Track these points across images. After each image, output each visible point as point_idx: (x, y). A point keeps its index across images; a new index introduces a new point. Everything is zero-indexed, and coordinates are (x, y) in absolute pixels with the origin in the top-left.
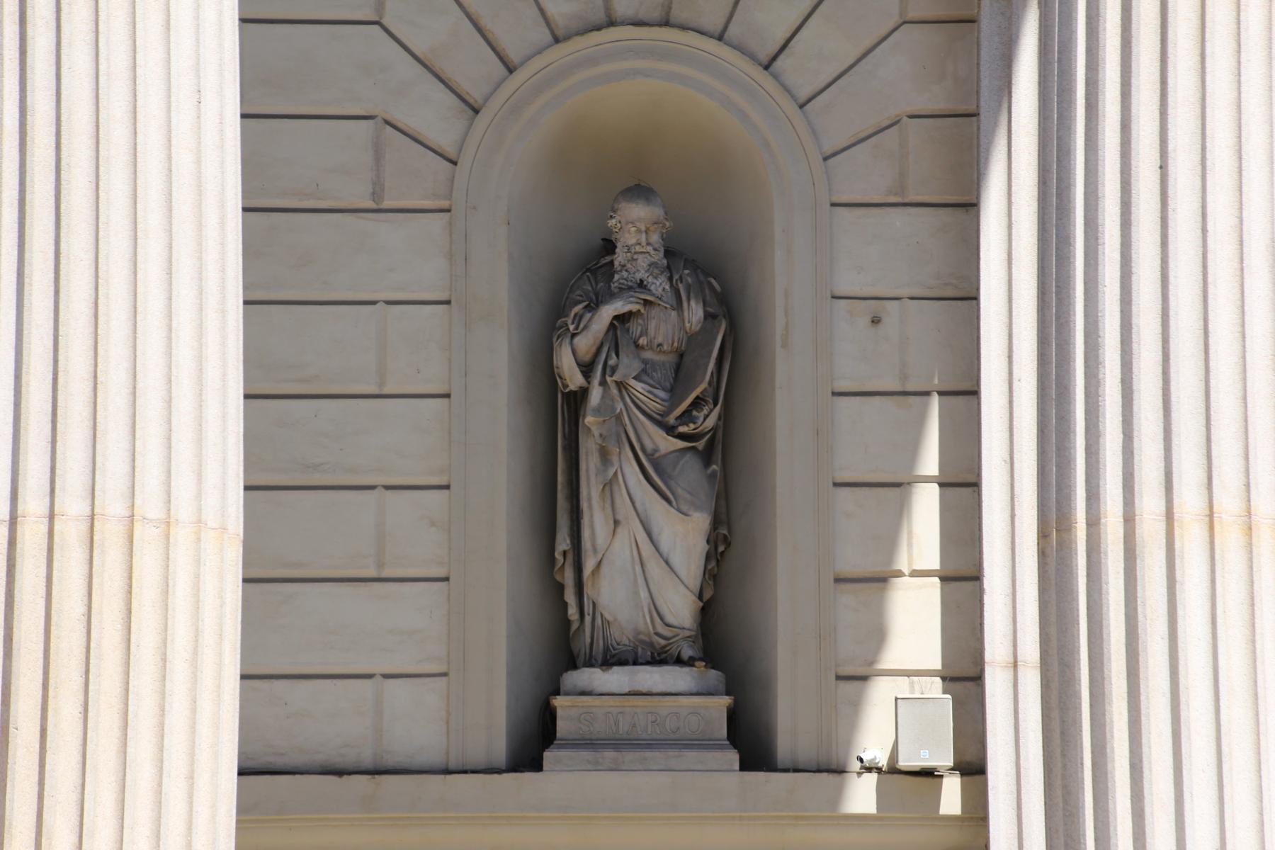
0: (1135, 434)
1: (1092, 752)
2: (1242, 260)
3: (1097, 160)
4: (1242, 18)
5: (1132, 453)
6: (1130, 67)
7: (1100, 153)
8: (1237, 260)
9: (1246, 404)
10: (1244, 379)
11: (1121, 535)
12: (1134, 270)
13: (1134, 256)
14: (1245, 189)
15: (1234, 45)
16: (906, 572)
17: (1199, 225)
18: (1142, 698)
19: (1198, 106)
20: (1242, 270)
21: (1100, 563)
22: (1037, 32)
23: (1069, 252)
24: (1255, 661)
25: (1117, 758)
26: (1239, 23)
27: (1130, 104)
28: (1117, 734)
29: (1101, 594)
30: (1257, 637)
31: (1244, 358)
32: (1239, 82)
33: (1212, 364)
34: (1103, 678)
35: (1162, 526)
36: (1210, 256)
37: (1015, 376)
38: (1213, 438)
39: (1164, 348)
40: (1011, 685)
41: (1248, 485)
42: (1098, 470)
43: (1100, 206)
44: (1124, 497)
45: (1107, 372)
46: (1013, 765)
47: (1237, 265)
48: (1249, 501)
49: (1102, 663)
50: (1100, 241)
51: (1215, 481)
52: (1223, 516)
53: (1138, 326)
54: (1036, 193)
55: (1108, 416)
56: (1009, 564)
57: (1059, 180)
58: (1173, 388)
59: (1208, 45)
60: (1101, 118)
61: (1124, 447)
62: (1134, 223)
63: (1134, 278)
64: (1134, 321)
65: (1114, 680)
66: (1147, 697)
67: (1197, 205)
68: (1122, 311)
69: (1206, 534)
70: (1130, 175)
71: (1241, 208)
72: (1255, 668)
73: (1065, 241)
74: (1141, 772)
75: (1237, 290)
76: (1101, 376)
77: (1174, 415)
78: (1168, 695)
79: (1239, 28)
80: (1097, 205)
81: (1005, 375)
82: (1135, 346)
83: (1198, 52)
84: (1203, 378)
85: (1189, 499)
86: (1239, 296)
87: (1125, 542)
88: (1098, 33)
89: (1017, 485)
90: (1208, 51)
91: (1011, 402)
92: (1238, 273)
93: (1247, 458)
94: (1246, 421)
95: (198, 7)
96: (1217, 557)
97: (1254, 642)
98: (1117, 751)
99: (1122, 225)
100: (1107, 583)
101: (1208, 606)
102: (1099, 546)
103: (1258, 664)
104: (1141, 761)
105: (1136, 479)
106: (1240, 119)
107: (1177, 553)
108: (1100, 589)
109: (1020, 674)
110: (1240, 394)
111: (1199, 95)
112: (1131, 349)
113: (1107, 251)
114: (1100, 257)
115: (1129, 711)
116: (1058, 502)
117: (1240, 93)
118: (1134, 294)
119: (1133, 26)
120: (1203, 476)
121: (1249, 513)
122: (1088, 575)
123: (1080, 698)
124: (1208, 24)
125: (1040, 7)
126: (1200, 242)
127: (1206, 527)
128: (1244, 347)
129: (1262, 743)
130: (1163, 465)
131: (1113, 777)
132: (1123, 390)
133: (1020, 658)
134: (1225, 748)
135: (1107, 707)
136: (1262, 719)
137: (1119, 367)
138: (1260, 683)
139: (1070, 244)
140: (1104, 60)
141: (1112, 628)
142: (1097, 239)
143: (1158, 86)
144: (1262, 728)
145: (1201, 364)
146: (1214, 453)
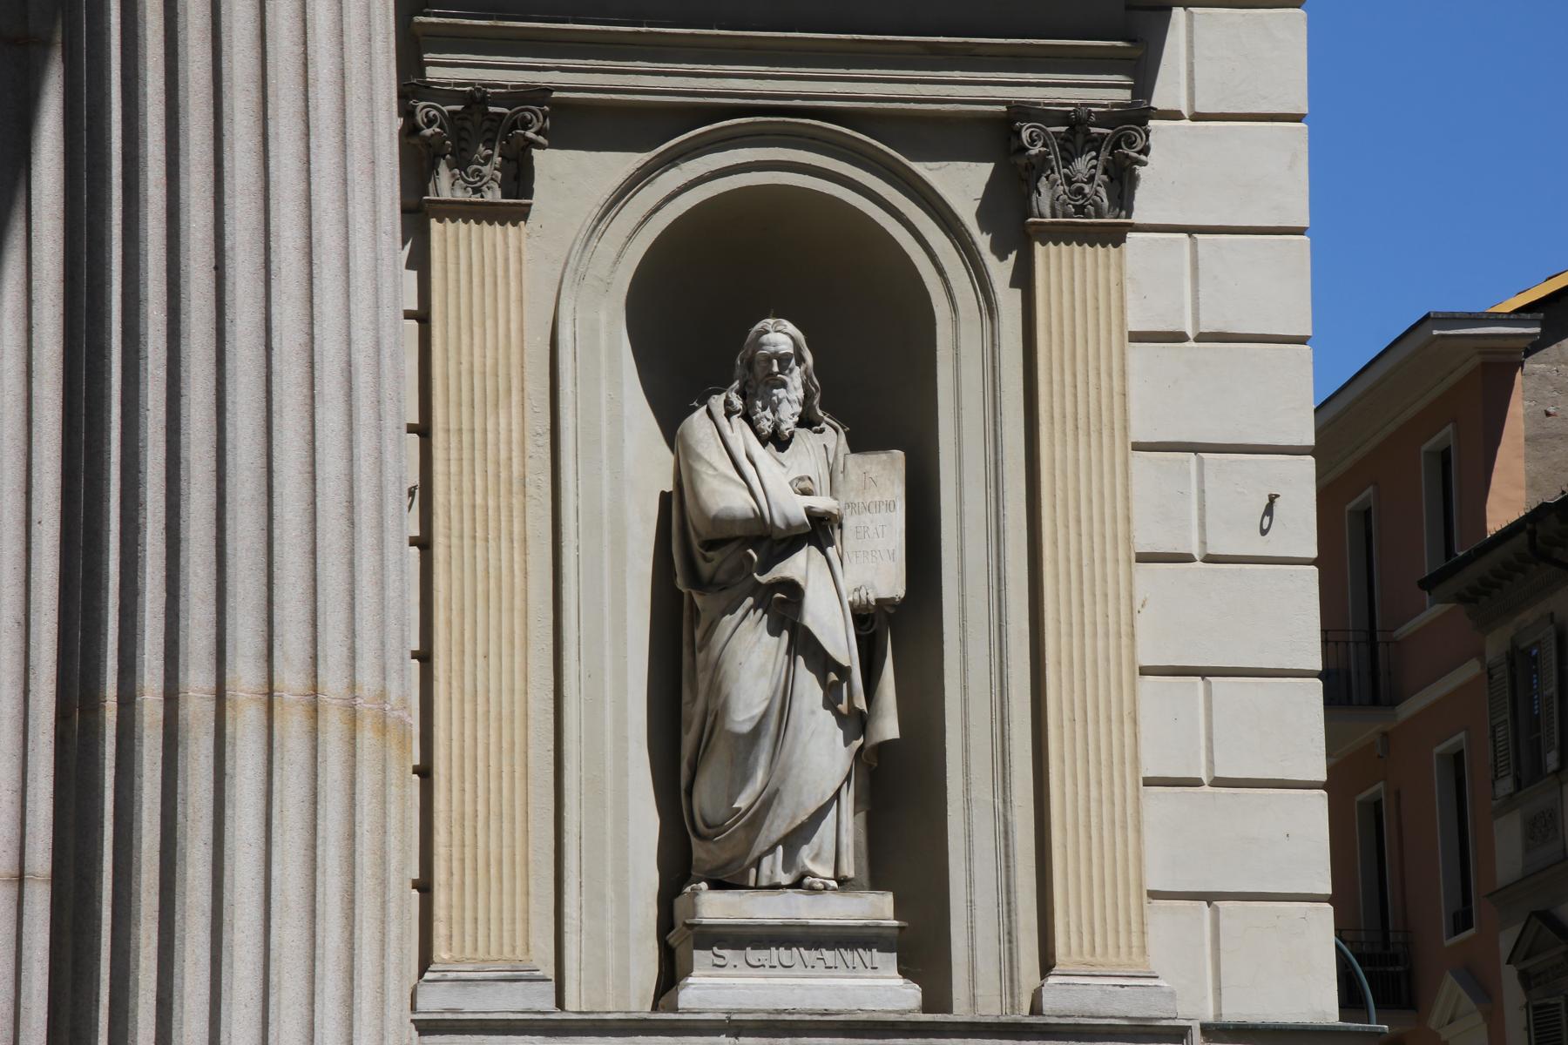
0: (182, 592)
1: (111, 986)
2: (312, 386)
3: (138, 254)
4: (310, 95)
5: (177, 616)
6: (177, 143)
7: (142, 245)
8: (307, 384)
9: (315, 559)
10: (314, 530)
11: (160, 716)
12: (183, 392)
13: (183, 375)
14: (316, 300)
15: (302, 126)
16: (1190, 334)
17: (262, 341)
18: (177, 917)
19: (260, 196)
20: (313, 397)
21: (133, 750)
22: (61, 90)
23: (103, 365)
24: (315, 870)
25: (141, 992)
26: (306, 100)
27: (178, 188)
28: (143, 963)
29: (132, 789)
30: (319, 842)
31: (314, 503)
32: (308, 171)
33: (276, 510)
34: (130, 894)
35: (210, 707)
36: (275, 379)
37: (35, 517)
38: (276, 599)
39: (218, 488)
40: (14, 904)
41: (315, 658)
42: (134, 636)
43: (142, 311)
44: (166, 670)
45: (149, 515)
46: (11, 1004)
47: (306, 391)
48: (316, 676)
49: (130, 875)
50: (142, 354)
51: (276, 653)
52: (285, 695)
53: (188, 461)
54: (61, 290)
55: (149, 570)
56: (19, 752)
57: (91, 276)
58: (229, 538)
59: (271, 123)
60: (142, 203)
61: (167, 608)
62: (184, 334)
63: (183, 401)
64: (183, 454)
65: (144, 896)
66: (183, 917)
67: (259, 317)
68: (168, 442)
69: (263, 717)
70: (178, 275)
71: (311, 324)
72: (314, 879)
73: (99, 353)
74: (171, 1009)
75: (306, 422)
76: (141, 521)
77: (230, 571)
78: (209, 914)
79: (307, 106)
80: (138, 309)
81: (21, 516)
82: (183, 485)
83: (259, 131)
84: (264, 526)
85: (245, 674)
86: (309, 429)
87: (165, 726)
88: (137, 98)
89: (33, 653)
90: (271, 130)
91: (28, 550)
92: (308, 401)
93: (315, 626)
94: (315, 580)
95: (368, 7)
96: (276, 745)
97: (314, 847)
98: (142, 984)
99: (169, 336)
100: (141, 776)
101: (261, 805)
102: (133, 731)
103: (318, 873)
104: (171, 996)
105: (182, 649)
106: (310, 216)
107: (228, 739)
108: (132, 783)
109: (27, 890)
110: (308, 548)
111: (260, 184)
112: (179, 489)
113: (150, 367)
114: (142, 374)
115: (160, 934)
116: (82, 675)
117: (309, 184)
118: (183, 421)
119: (181, 93)
120: (262, 646)
121: (316, 691)
122: (117, 766)
123: (100, 919)
124: (271, 99)
125: (64, 61)
126: (262, 361)
127: (263, 708)
128: (314, 490)
129: (318, 970)
130: (214, 631)
131: (136, 1016)
132: (168, 538)
133: (27, 870)
134: (273, 978)
135: (133, 930)
136: (319, 941)
137: (163, 510)
138: (319, 897)
139: (104, 357)
140: (145, 131)
141: (144, 832)
142: (138, 351)
143: (211, 169)
144: (319, 951)
145: (263, 509)
146: (276, 619)
